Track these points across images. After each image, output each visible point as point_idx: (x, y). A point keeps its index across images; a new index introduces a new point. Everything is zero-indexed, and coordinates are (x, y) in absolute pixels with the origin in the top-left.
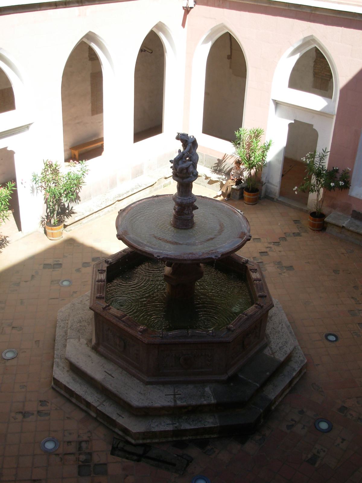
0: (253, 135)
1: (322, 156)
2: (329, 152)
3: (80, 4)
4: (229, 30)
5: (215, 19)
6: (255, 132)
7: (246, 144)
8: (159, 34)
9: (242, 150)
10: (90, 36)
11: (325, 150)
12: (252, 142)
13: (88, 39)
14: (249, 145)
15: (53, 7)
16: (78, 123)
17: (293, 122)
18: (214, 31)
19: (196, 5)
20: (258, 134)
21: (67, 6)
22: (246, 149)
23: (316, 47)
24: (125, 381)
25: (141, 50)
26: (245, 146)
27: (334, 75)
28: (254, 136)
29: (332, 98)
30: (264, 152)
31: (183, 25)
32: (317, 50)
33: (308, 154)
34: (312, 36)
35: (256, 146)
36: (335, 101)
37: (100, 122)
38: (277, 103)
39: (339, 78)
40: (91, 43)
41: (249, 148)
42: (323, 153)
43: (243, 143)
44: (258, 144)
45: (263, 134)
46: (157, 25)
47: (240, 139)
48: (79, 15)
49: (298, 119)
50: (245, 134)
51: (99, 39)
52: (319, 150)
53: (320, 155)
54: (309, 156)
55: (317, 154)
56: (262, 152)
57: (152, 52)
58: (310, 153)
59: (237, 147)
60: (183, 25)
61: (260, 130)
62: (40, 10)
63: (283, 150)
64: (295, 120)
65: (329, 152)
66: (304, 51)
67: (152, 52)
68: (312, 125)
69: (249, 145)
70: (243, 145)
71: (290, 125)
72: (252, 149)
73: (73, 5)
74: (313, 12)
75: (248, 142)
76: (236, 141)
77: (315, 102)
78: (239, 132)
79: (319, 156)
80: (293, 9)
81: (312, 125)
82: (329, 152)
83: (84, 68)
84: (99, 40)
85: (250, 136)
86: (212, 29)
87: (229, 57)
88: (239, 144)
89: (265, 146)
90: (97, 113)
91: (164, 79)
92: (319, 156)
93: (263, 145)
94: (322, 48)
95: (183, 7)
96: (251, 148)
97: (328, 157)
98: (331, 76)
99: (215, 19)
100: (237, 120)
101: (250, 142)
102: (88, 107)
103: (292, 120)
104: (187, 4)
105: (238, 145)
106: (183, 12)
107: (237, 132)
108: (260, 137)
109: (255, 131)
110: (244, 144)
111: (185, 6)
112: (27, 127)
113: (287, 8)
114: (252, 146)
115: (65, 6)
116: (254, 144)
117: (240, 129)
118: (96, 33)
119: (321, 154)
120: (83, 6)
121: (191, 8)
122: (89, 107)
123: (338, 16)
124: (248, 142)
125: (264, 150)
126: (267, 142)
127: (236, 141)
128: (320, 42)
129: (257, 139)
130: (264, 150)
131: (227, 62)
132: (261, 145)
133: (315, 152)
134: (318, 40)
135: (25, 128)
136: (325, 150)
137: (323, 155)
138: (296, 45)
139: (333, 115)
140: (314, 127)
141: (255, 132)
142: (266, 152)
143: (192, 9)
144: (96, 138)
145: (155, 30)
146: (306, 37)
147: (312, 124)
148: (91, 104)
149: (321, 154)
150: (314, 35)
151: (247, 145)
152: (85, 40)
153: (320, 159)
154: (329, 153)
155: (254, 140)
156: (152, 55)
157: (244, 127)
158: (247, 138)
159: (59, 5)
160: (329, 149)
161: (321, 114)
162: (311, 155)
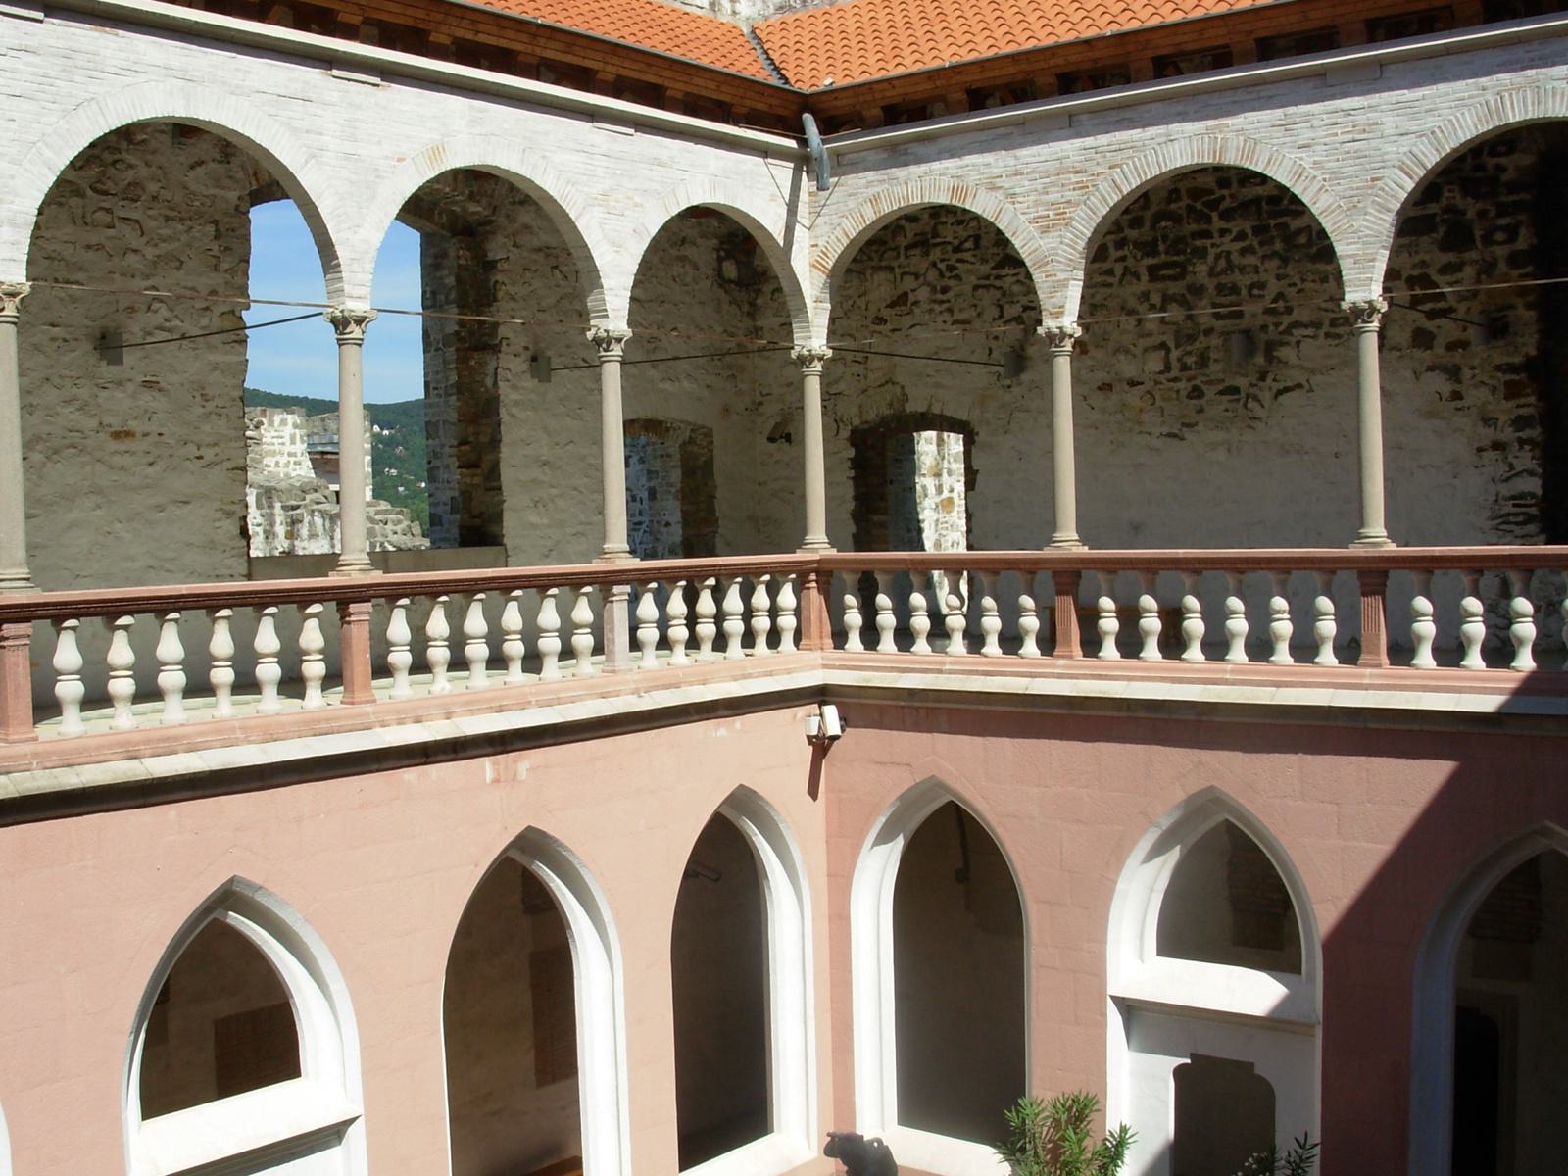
0: (1064, 1117)
1: (1298, 1160)
2: (1318, 1148)
3: (499, 749)
4: (955, 794)
5: (908, 765)
6: (1071, 1107)
7: (1043, 1148)
8: (742, 823)
9: (1036, 1168)
10: (532, 844)
11: (1303, 1141)
12: (1064, 1138)
13: (523, 850)
14: (1056, 1151)
15: (417, 761)
16: (494, 1114)
17: (1188, 1061)
18: (908, 801)
19: (848, 730)
20: (1081, 1112)
21: (460, 755)
22: (1047, 1163)
23: (1227, 820)
24: (734, 13)
25: (689, 874)
26: (1041, 1153)
27: (1296, 897)
28: (1069, 1118)
29: (1300, 973)
30: (1107, 1169)
31: (813, 791)
32: (1229, 827)
33: (1251, 1160)
34: (1211, 788)
35: (1077, 1150)
36: (1311, 979)
37: (563, 1108)
38: (1128, 1006)
39: (1315, 906)
40: (533, 863)
41: (1055, 1159)
42: (1300, 1151)
43: (1035, 1147)
44: (1084, 1144)
45: (1098, 1111)
46: (732, 795)
47: (1023, 1134)
48: (496, 781)
49: (1204, 1051)
50: (1037, 1115)
51: (559, 849)
52: (1284, 1143)
53: (1291, 1160)
54: (1254, 1166)
55: (1281, 1154)
56: (1100, 1168)
57: (718, 880)
58: (1255, 1155)
59: (1018, 1161)
60: (813, 791)
61: (1086, 1097)
62: (378, 771)
63: (1168, 1157)
64: (1193, 1056)
65: (1317, 1145)
66: (1192, 839)
67: (718, 880)
68: (1252, 1065)
69: (1056, 1151)
70: (1036, 1154)
71: (1179, 1073)
72: (1066, 1164)
73: (475, 752)
74: (1205, 718)
75: (1050, 1141)
76: (1013, 1143)
77: (1247, 991)
78: (1018, 1112)
79: (1289, 1163)
80: (1142, 714)
81: (1252, 1065)
82: (1318, 1148)
83: (511, 956)
84: (560, 852)
85: (1055, 1120)
86: (901, 798)
87: (963, 876)
88: (1023, 1150)
89: (1107, 1148)
90: (554, 1079)
91: (768, 1055)
92: (1289, 1163)
93: (1099, 1146)
94: (1248, 823)
95: (809, 738)
96: (1063, 1158)
97: (1317, 1160)
98: (1286, 904)
99: (908, 765)
100: (1010, 1077)
101: (1060, 1139)
102: (526, 1059)
103: (1185, 1057)
104: (820, 727)
105: (1018, 1155)
106: (808, 751)
107: (1010, 1112)
108: (1089, 1122)
109: (1070, 1102)
110: (1039, 1150)
111: (815, 732)
112: (333, 1134)
113: (1124, 714)
114: (1065, 1152)
115: (452, 756)
116: (1070, 1149)
117: (1020, 1101)
118: (551, 832)
119: (1293, 1154)
120: (507, 752)
121: (835, 738)
122: (529, 1060)
123: (1281, 722)
124: (1050, 1141)
125: (1106, 1160)
126: (1112, 1135)
127: (1013, 1143)
128: (1238, 803)
129: (1078, 1127)
130: (1106, 1160)
131: (961, 900)
132: (1095, 1146)
133: (1272, 1150)
134: (1232, 799)
135: (327, 1136)
136: (1303, 1141)
137: (1301, 1158)
138: (1166, 823)
139: (1313, 1026)
140: (1258, 1071)
141: (1071, 1107)
142: (1112, 1167)
143: (836, 742)
144: (554, 1161)
145: (729, 814)
146: (1194, 795)
147: (1251, 1060)
148: (532, 1053)
149: (1293, 1154)
150: (1216, 784)
151: (1050, 1151)
152: (516, 855)
153: (1293, 1170)
154: (1317, 1150)
155: (1070, 1132)
156: (721, 891)
157: (1034, 1093)
158: (1045, 1129)
159: (436, 754)
160: (1316, 1137)
161: (1273, 1024)
162: (1258, 1161)
